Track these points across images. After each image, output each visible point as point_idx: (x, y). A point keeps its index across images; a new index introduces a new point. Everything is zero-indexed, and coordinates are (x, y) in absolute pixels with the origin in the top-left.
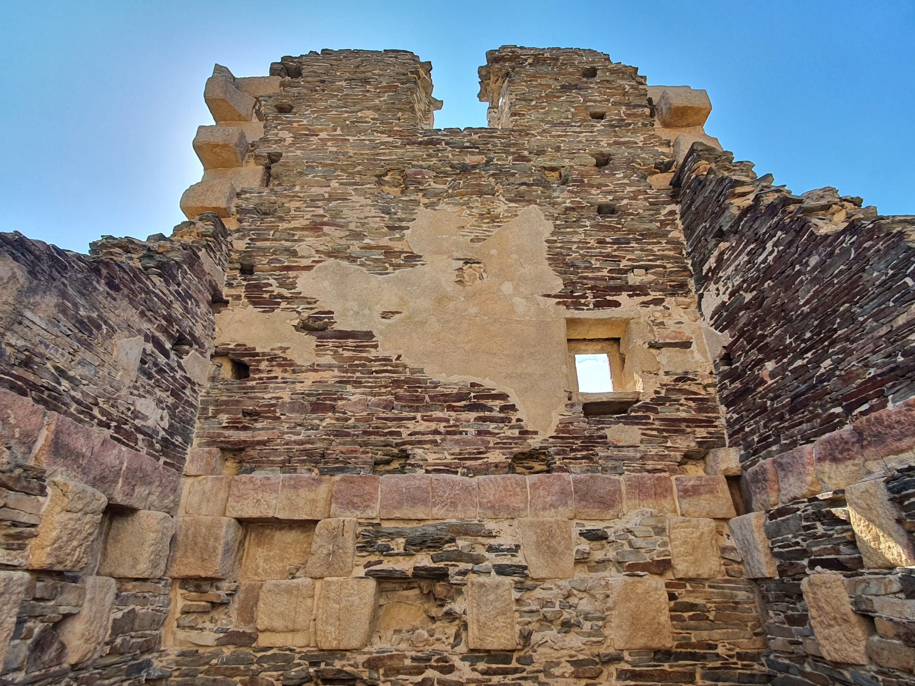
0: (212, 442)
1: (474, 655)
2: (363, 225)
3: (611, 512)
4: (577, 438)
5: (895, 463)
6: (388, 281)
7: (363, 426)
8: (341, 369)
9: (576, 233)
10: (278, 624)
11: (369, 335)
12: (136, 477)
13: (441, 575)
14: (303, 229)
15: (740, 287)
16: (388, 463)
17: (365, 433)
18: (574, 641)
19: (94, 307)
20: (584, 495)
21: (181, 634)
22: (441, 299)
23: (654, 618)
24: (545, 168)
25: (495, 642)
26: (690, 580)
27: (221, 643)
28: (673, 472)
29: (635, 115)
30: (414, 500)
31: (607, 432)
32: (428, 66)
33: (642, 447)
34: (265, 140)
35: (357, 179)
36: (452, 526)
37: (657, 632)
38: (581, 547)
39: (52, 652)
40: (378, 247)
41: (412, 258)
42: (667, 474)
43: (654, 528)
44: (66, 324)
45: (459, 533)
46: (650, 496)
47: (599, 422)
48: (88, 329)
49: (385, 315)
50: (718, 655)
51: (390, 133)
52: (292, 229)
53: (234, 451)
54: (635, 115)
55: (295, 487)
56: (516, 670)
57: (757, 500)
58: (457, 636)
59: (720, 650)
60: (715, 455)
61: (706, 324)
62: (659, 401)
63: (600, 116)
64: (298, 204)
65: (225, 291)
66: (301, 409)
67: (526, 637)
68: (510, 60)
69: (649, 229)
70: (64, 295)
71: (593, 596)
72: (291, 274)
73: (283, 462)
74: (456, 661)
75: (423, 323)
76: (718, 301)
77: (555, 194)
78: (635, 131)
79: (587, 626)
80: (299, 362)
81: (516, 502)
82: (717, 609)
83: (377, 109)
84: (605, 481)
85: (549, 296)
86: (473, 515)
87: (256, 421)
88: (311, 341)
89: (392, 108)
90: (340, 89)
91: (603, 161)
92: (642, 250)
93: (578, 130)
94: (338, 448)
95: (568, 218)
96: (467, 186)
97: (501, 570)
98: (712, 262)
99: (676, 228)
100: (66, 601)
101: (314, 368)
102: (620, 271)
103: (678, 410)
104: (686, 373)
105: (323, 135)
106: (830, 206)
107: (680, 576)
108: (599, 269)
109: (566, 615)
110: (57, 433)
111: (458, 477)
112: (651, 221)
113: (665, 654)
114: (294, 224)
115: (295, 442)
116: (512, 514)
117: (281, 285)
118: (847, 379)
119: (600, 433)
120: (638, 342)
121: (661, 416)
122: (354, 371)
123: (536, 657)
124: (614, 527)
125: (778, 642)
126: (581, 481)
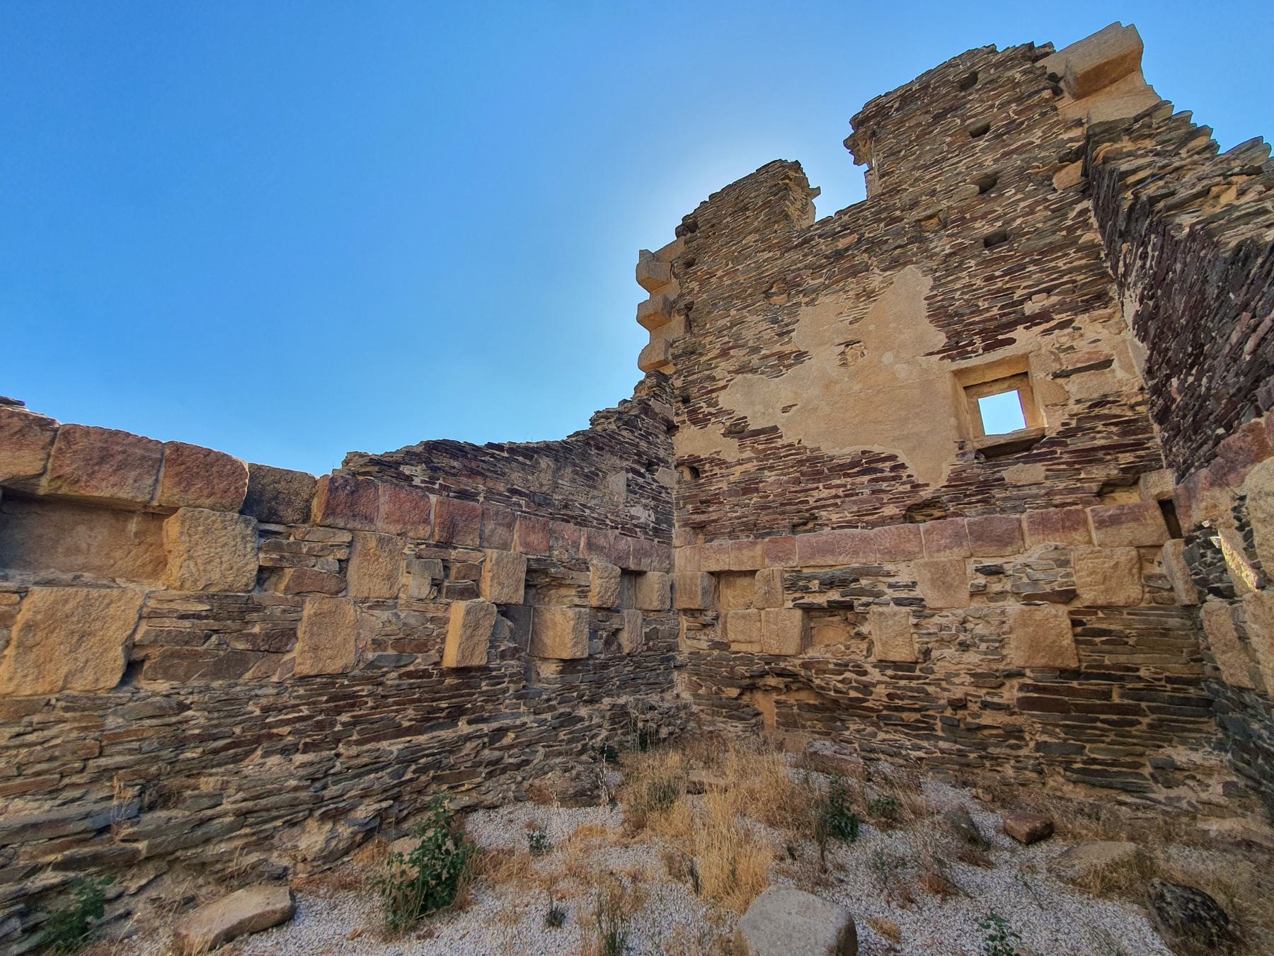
1: (882, 664)
2: (758, 339)
3: (1010, 549)
4: (971, 484)
7: (780, 500)
9: (958, 278)
10: (741, 638)
11: (775, 429)
12: (640, 553)
13: (849, 607)
16: (805, 524)
17: (782, 504)
18: (972, 658)
19: (592, 465)
20: (981, 536)
21: (689, 642)
22: (829, 385)
23: (1054, 642)
24: (920, 221)
26: (1102, 608)
27: (711, 648)
28: (1088, 503)
29: (1030, 108)
31: (1004, 474)
32: (797, 166)
33: (1048, 483)
34: (681, 296)
36: (854, 569)
38: (976, 582)
39: (614, 647)
40: (773, 355)
41: (800, 356)
42: (1080, 507)
43: (1056, 561)
44: (579, 480)
45: (862, 575)
46: (1058, 530)
47: (995, 466)
48: (592, 479)
49: (785, 410)
50: (1139, 677)
51: (770, 249)
53: (699, 528)
54: (1030, 108)
55: (739, 549)
56: (919, 678)
59: (1142, 673)
60: (1145, 481)
62: (1068, 432)
65: (676, 420)
66: (736, 494)
67: (927, 653)
69: (1051, 243)
70: (574, 465)
71: (988, 622)
72: (714, 395)
77: (932, 246)
80: (729, 460)
81: (910, 547)
82: (1139, 635)
83: (757, 230)
84: (1001, 523)
85: (931, 354)
86: (873, 560)
88: (735, 443)
89: (768, 223)
90: (727, 227)
92: (1041, 271)
93: (956, 160)
94: (764, 518)
96: (841, 272)
97: (899, 602)
99: (1091, 228)
100: (615, 623)
101: (740, 463)
102: (1014, 304)
103: (1094, 438)
104: (1106, 396)
105: (719, 273)
106: (1209, 191)
107: (1087, 604)
108: (988, 310)
109: (962, 637)
110: (589, 538)
111: (859, 530)
112: (1054, 233)
113: (1066, 673)
114: (710, 355)
116: (909, 557)
119: (997, 475)
120: (1039, 376)
121: (1071, 448)
122: (768, 458)
123: (936, 668)
124: (1011, 561)
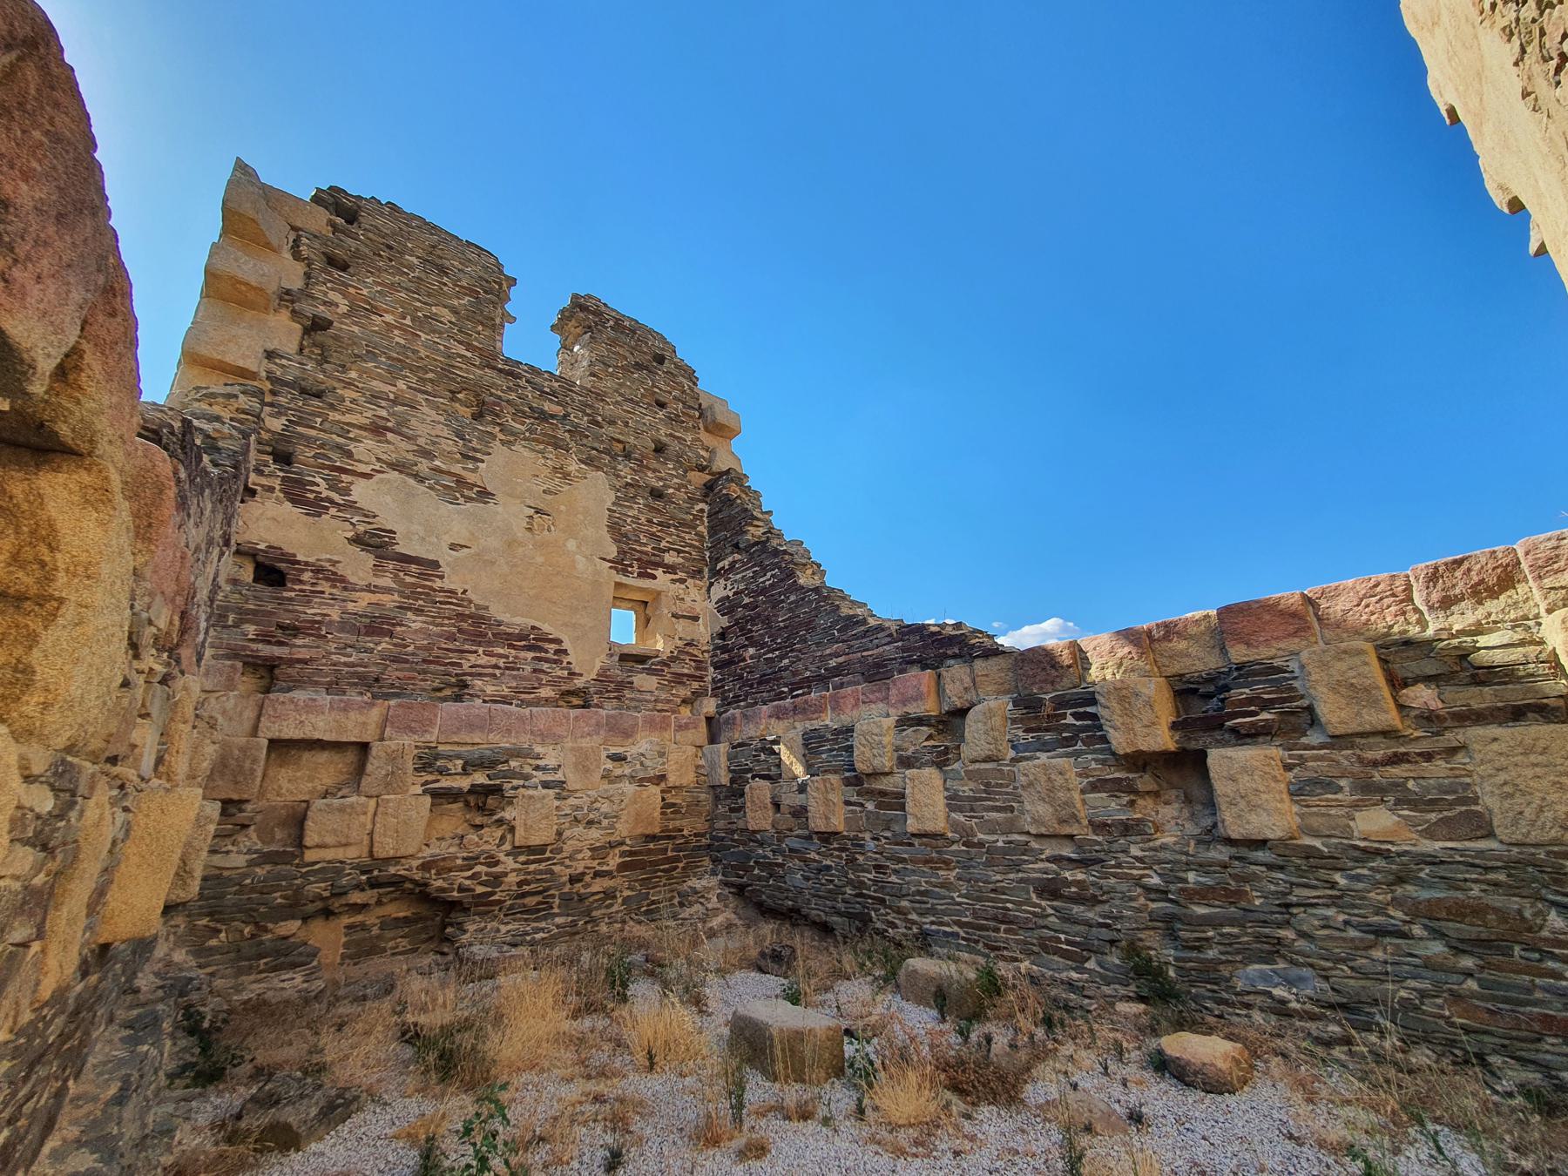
0: (233, 654)
2: (434, 443)
5: (809, 725)
6: (459, 513)
7: (423, 654)
8: (401, 594)
10: (329, 840)
11: (435, 565)
13: (497, 790)
14: (360, 428)
15: (742, 592)
17: (424, 661)
18: (594, 833)
22: (511, 544)
25: (535, 840)
28: (674, 712)
30: (471, 727)
31: (634, 679)
35: (429, 388)
37: (651, 824)
40: (449, 473)
41: (484, 495)
49: (453, 547)
51: (469, 347)
52: (348, 424)
57: (724, 736)
58: (503, 838)
59: (685, 832)
61: (711, 606)
62: (673, 659)
63: (662, 405)
64: (355, 395)
67: (559, 834)
68: (594, 313)
73: (330, 684)
74: (502, 857)
75: (493, 563)
76: (724, 593)
78: (686, 430)
79: (605, 822)
80: (352, 579)
81: (559, 731)
83: (455, 311)
86: (524, 741)
87: (295, 636)
88: (369, 560)
91: (660, 449)
94: (393, 673)
95: (628, 492)
97: (546, 785)
98: (726, 563)
101: (370, 589)
102: (660, 550)
105: (389, 318)
113: (652, 838)
114: (348, 418)
115: (345, 664)
116: (557, 740)
117: (330, 488)
118: (794, 674)
124: (631, 751)
125: (721, 824)
126: (612, 716)
